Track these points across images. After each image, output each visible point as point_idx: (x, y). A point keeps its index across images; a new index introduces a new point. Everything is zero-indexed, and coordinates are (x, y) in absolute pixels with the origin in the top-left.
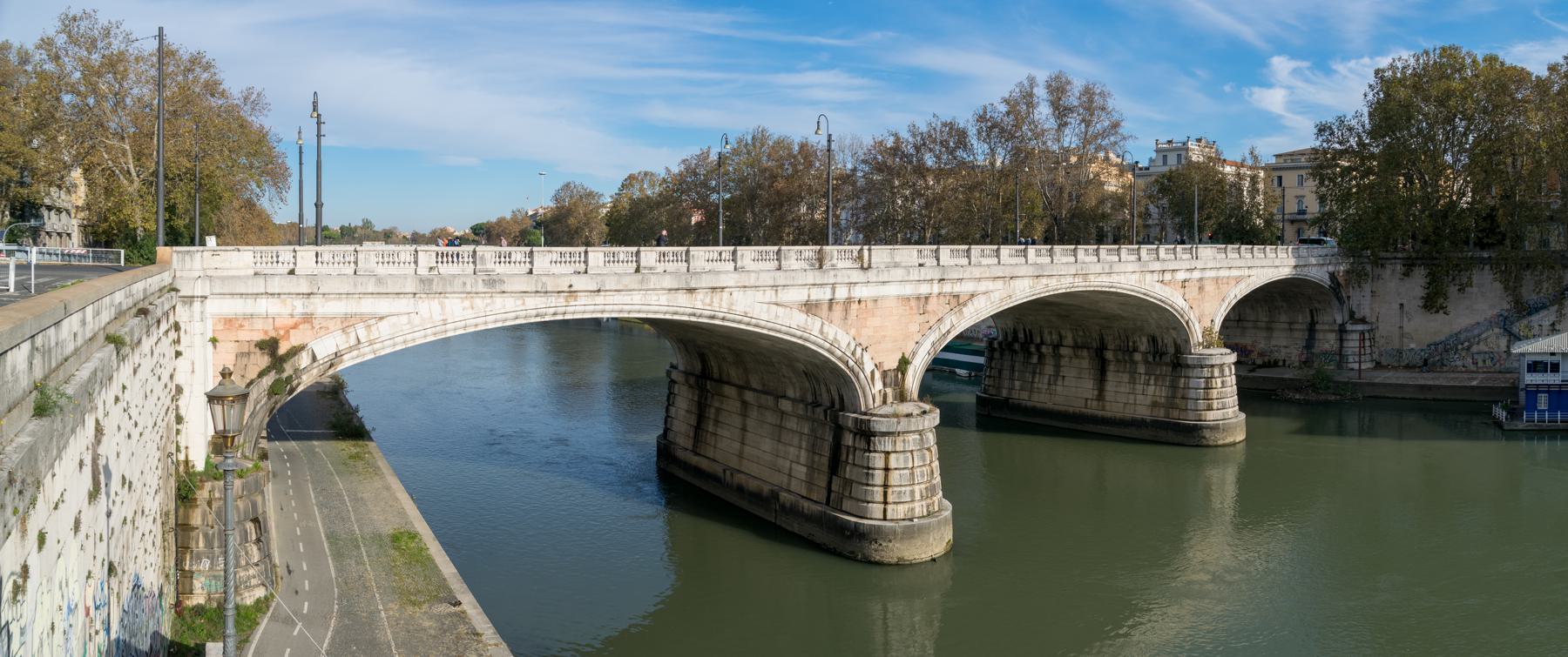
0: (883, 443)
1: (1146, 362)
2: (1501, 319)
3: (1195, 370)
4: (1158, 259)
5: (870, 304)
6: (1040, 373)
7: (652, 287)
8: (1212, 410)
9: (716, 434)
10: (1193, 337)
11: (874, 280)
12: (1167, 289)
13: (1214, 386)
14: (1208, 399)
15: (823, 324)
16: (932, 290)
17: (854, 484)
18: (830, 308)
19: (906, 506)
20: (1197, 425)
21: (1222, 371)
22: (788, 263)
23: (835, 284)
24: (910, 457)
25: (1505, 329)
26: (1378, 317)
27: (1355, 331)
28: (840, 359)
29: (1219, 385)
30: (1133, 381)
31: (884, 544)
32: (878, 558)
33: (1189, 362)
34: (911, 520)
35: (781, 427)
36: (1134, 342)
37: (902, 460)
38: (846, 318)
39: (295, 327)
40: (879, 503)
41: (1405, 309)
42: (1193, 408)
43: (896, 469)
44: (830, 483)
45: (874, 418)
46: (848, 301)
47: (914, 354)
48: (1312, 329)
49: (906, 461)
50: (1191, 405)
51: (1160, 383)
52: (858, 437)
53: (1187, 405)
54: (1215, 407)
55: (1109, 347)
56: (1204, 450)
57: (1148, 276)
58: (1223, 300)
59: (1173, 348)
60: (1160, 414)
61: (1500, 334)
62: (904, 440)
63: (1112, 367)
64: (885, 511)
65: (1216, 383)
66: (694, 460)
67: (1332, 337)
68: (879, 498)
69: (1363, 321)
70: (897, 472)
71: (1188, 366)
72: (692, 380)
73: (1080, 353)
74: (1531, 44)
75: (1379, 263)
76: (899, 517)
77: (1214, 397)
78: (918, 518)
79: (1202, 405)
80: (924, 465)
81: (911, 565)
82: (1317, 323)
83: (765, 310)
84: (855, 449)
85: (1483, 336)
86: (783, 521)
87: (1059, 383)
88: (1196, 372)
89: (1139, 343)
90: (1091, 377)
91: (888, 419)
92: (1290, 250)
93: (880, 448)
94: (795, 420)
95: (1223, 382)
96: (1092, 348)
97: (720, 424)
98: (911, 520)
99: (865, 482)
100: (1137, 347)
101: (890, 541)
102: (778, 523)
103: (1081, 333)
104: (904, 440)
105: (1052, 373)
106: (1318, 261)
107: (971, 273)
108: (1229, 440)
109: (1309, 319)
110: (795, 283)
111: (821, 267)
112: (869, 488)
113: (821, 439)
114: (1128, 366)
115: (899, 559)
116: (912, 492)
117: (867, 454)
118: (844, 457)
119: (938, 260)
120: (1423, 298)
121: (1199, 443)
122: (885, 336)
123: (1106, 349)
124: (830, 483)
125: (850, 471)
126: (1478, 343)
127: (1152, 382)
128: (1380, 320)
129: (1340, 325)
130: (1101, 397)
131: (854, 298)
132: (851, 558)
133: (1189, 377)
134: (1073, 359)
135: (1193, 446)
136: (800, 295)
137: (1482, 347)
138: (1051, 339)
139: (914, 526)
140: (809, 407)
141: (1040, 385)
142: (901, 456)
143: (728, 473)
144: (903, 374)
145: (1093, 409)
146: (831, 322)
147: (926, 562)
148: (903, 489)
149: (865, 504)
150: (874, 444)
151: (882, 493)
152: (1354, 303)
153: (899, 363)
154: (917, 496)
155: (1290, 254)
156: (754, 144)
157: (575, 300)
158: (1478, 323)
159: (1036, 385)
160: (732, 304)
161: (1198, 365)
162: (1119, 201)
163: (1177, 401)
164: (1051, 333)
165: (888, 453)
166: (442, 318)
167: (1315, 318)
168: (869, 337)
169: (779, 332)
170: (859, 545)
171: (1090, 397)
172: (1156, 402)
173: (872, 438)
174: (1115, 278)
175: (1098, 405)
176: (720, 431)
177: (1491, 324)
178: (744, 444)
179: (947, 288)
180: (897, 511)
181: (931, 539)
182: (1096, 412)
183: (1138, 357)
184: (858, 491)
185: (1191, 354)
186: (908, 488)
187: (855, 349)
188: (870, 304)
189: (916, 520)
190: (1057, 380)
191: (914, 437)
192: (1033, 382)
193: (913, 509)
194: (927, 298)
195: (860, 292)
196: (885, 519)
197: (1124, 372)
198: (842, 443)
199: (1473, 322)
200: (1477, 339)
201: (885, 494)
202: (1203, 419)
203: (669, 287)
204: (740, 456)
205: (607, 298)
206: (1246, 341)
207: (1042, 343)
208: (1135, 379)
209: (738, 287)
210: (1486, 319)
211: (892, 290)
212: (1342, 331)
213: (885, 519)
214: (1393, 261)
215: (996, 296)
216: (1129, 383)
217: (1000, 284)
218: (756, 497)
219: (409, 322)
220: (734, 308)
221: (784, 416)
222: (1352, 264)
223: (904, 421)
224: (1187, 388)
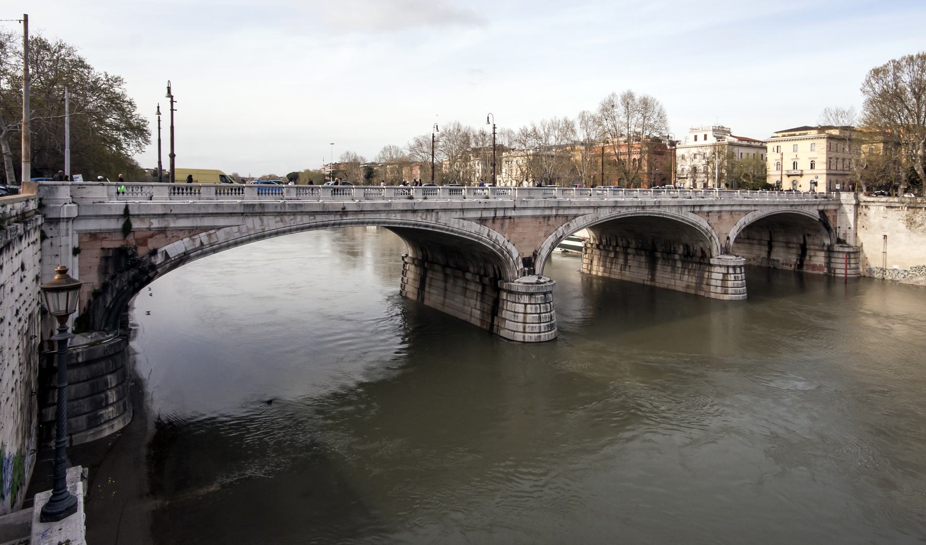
1: (683, 262)
7: (392, 209)
8: (728, 294)
9: (430, 293)
13: (729, 279)
15: (489, 230)
18: (494, 222)
23: (497, 208)
27: (843, 252)
30: (674, 270)
37: (534, 309)
39: (152, 236)
46: (504, 218)
49: (536, 309)
51: (692, 274)
55: (658, 250)
72: (416, 262)
80: (547, 312)
83: (457, 222)
84: (508, 301)
87: (627, 269)
97: (432, 287)
105: (623, 263)
109: (802, 242)
122: (524, 238)
123: (657, 251)
127: (686, 273)
130: (653, 280)
131: (507, 216)
133: (711, 272)
138: (622, 244)
141: (616, 270)
142: (534, 306)
148: (534, 325)
157: (347, 216)
159: (613, 270)
161: (718, 265)
164: (622, 240)
166: (262, 228)
168: (515, 238)
171: (647, 279)
186: (537, 325)
190: (626, 268)
191: (541, 296)
192: (611, 268)
197: (668, 266)
203: (402, 209)
205: (366, 215)
208: (675, 270)
212: (830, 251)
216: (671, 272)
217: (591, 211)
219: (239, 231)
220: (439, 221)
224: (709, 278)
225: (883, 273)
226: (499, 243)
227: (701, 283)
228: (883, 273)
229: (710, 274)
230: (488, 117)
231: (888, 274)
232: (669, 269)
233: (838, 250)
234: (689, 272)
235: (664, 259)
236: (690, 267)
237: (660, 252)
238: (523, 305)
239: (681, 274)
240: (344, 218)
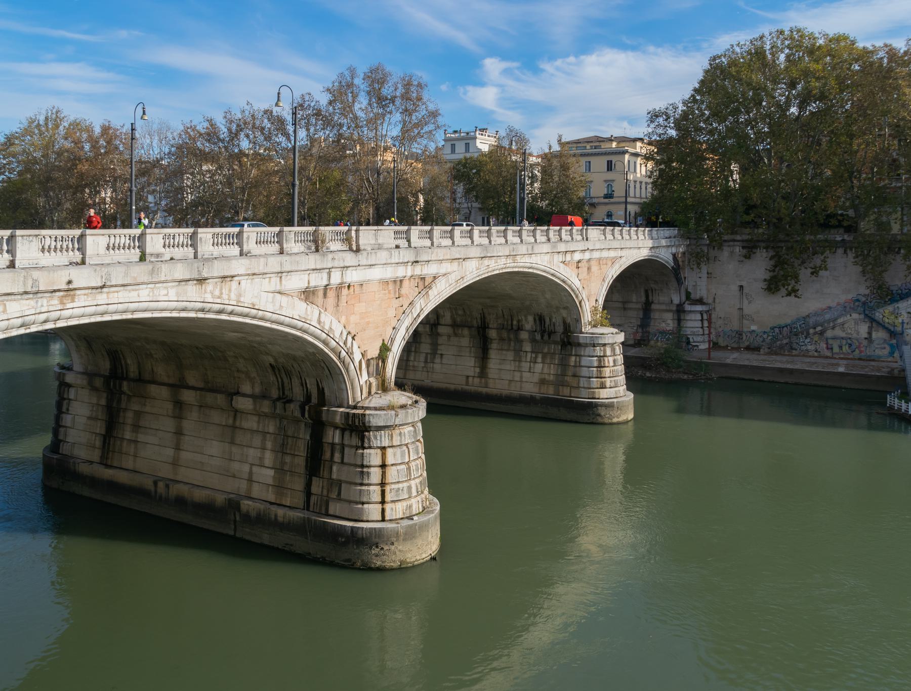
0: (378, 438)
1: (533, 341)
2: (857, 304)
3: (587, 349)
4: (561, 239)
5: (357, 288)
6: (416, 352)
8: (605, 388)
9: (136, 442)
10: (584, 317)
11: (365, 263)
12: (567, 269)
14: (601, 378)
16: (406, 272)
17: (343, 485)
19: (404, 504)
20: (592, 402)
21: (613, 350)
22: (289, 245)
24: (407, 451)
25: (866, 315)
26: (714, 298)
28: (333, 350)
29: (611, 364)
30: (518, 359)
31: (386, 548)
32: (379, 563)
33: (581, 341)
34: (410, 518)
35: (234, 427)
36: (519, 321)
38: (338, 306)
40: (376, 503)
41: (744, 291)
42: (586, 386)
43: (392, 465)
44: (308, 485)
45: (368, 412)
46: (340, 287)
47: (392, 340)
48: (647, 308)
49: (403, 455)
50: (583, 383)
51: (548, 361)
52: (347, 434)
53: (579, 383)
54: (608, 385)
55: (490, 326)
56: (599, 427)
57: (556, 256)
58: (603, 280)
59: (562, 327)
60: (550, 391)
61: (860, 319)
62: (400, 434)
63: (494, 345)
64: (383, 511)
66: (107, 474)
67: (669, 316)
68: (377, 497)
69: (700, 301)
70: (394, 468)
71: (579, 345)
73: (460, 332)
74: (736, 34)
75: (717, 243)
76: (398, 517)
77: (607, 376)
78: (417, 514)
79: (595, 383)
81: (414, 566)
82: (652, 302)
85: (840, 321)
86: (245, 533)
87: (437, 360)
88: (589, 351)
89: (524, 322)
90: (472, 355)
91: (385, 412)
92: (646, 231)
93: (375, 443)
94: (256, 418)
95: (614, 361)
96: (473, 327)
98: (410, 518)
99: (359, 481)
101: (393, 544)
102: (238, 535)
103: (460, 312)
104: (400, 434)
105: (429, 351)
106: (666, 242)
107: (437, 255)
108: (623, 418)
109: (643, 299)
110: (299, 268)
111: (317, 250)
112: (363, 488)
113: (293, 437)
114: (512, 344)
115: (401, 562)
116: (410, 488)
117: (361, 451)
118: (327, 455)
119: (409, 241)
120: (765, 280)
121: (594, 421)
122: (368, 323)
123: (488, 328)
124: (308, 485)
125: (338, 471)
126: (833, 328)
127: (539, 360)
128: (717, 301)
129: (678, 305)
132: (348, 566)
133: (580, 356)
134: (452, 338)
135: (583, 423)
136: (297, 282)
137: (838, 332)
139: (416, 524)
140: (278, 403)
141: (416, 364)
142: (398, 451)
143: (161, 485)
144: (384, 362)
145: (475, 386)
147: (427, 561)
148: (400, 486)
149: (360, 506)
150: (369, 440)
151: (380, 492)
152: (689, 283)
153: (380, 350)
154: (414, 493)
155: (646, 236)
157: (73, 301)
158: (830, 308)
159: (411, 364)
161: (591, 344)
163: (568, 379)
165: (383, 449)
167: (650, 298)
169: (281, 324)
170: (357, 551)
171: (472, 374)
172: (545, 379)
173: (367, 434)
174: (534, 259)
176: (141, 438)
177: (846, 309)
178: (180, 449)
179: (418, 270)
180: (395, 510)
181: (430, 537)
182: (480, 389)
183: (524, 335)
184: (347, 492)
185: (581, 333)
186: (405, 485)
187: (346, 338)
188: (357, 288)
189: (415, 518)
190: (434, 357)
193: (411, 506)
194: (401, 281)
195: (353, 276)
196: (383, 520)
197: (508, 350)
198: (324, 440)
199: (824, 307)
200: (831, 324)
201: (383, 493)
202: (597, 397)
204: (175, 463)
205: (111, 295)
209: (249, 275)
210: (838, 304)
211: (377, 274)
212: (680, 311)
213: (383, 520)
214: (731, 243)
215: (453, 278)
218: (207, 509)
221: (239, 415)
222: (688, 246)
223: (402, 412)
224: (578, 366)
225: (739, 338)
226: (334, 334)
227: (564, 374)
228: (739, 338)
229: (578, 360)
230: (279, 94)
231: (744, 338)
232: (510, 355)
233: (689, 309)
234: (544, 358)
235: (502, 339)
236: (546, 350)
237: (494, 329)
238: (379, 451)
239: (530, 362)
240: (69, 306)
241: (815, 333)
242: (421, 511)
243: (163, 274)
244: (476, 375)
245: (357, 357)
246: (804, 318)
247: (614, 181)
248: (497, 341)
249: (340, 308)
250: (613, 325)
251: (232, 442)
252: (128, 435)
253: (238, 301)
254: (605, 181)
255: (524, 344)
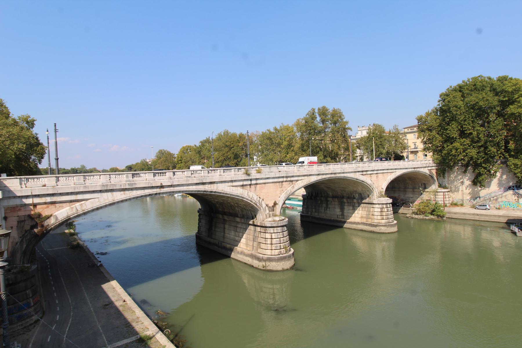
0: (270, 230)
15: (248, 192)
29: (386, 211)
37: (273, 252)
43: (274, 238)
47: (59, 186)
51: (364, 210)
65: (385, 210)
66: (209, 239)
87: (328, 210)
100: (355, 197)
105: (325, 206)
126: (501, 197)
146: (251, 191)
148: (277, 245)
156: (224, 135)
160: (218, 187)
162: (32, 215)
163: (371, 216)
171: (339, 214)
175: (342, 217)
197: (350, 206)
200: (501, 196)
206: (396, 195)
207: (322, 196)
216: (352, 210)
219: (99, 201)
220: (218, 188)
229: (373, 209)
232: (351, 208)
241: (493, 200)
242: (285, 253)
243: (190, 182)
244: (340, 215)
245: (264, 206)
246: (490, 194)
247: (416, 142)
248: (347, 203)
249: (257, 191)
250: (387, 197)
251: (236, 231)
252: (213, 229)
253: (217, 189)
254: (413, 143)
255: (356, 204)
